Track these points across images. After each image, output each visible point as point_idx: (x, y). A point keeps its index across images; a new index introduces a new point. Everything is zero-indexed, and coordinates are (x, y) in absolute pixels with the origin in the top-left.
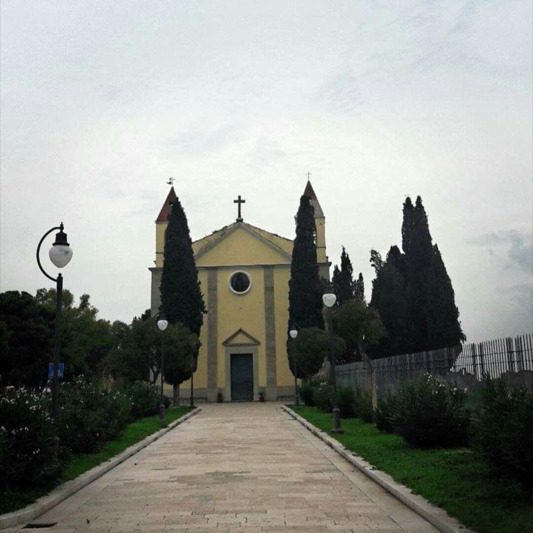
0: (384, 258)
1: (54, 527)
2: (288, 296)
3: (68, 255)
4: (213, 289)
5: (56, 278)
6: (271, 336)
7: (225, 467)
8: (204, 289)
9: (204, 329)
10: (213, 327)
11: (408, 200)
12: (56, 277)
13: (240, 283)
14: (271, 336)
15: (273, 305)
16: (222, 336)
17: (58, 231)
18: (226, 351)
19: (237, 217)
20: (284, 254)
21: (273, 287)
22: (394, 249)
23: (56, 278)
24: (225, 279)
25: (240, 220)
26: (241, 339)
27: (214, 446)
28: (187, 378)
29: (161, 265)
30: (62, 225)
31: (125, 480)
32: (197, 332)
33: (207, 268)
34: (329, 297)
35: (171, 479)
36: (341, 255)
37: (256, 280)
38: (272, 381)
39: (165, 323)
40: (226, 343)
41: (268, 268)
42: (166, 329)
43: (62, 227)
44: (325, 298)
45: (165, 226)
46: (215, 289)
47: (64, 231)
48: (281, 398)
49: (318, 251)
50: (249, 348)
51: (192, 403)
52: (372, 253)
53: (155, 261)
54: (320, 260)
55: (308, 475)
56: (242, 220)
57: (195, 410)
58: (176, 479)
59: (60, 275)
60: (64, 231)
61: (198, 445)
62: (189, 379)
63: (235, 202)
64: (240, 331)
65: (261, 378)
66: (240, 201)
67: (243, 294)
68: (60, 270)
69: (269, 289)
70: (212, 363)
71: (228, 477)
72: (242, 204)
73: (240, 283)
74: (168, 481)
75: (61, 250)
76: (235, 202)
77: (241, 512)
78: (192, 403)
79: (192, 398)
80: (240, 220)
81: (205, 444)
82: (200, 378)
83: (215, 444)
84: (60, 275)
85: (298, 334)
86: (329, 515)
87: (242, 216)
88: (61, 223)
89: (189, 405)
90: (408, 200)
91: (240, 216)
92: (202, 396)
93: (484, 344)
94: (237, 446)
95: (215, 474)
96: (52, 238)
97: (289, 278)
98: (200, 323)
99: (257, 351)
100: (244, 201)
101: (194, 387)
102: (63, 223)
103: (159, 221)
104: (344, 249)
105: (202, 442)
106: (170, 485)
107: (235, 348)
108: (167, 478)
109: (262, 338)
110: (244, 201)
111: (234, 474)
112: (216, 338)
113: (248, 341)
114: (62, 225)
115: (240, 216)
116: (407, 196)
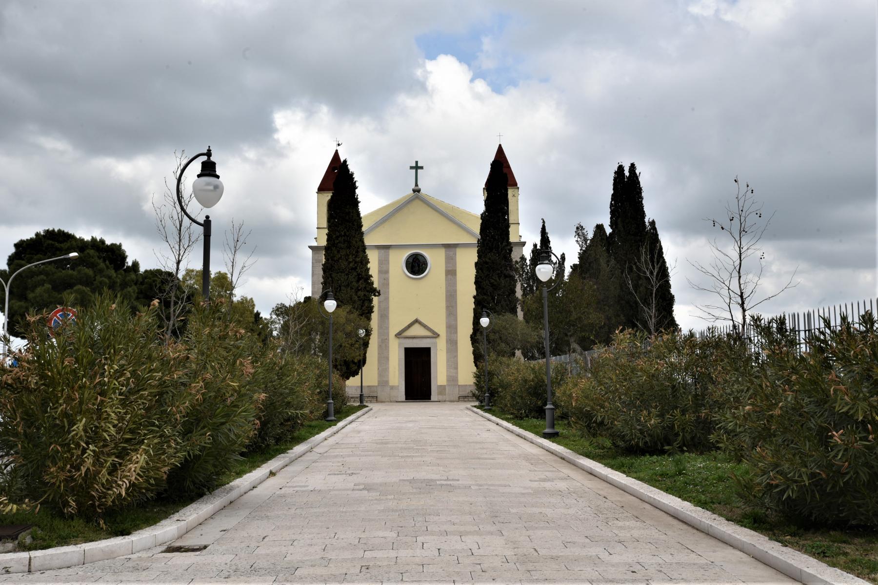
0: (590, 236)
1: (204, 551)
2: (473, 280)
3: (218, 190)
4: (384, 271)
5: (202, 222)
6: (452, 328)
7: (423, 474)
8: (373, 268)
9: (375, 316)
10: (384, 317)
11: (621, 168)
12: (201, 220)
13: (416, 265)
14: (452, 328)
15: (455, 291)
16: (395, 327)
17: (205, 158)
18: (400, 345)
19: (413, 186)
20: (469, 232)
21: (456, 270)
22: (600, 228)
23: (202, 222)
24: (398, 261)
25: (417, 191)
26: (416, 330)
27: (401, 448)
28: (355, 373)
29: (324, 243)
30: (209, 150)
31: (295, 487)
32: (369, 319)
33: (378, 247)
34: (543, 268)
35: (357, 487)
36: (541, 227)
37: (435, 260)
38: (453, 379)
39: (334, 304)
40: (398, 335)
41: (449, 247)
42: (333, 312)
43: (209, 154)
44: (539, 270)
45: (328, 196)
46: (387, 272)
47: (212, 159)
48: (463, 398)
49: (512, 229)
50: (428, 340)
51: (361, 401)
52: (577, 228)
53: (316, 238)
54: (513, 239)
55: (535, 485)
56: (419, 191)
57: (366, 409)
58: (362, 487)
59: (207, 217)
60: (212, 159)
61: (378, 446)
62: (357, 374)
63: (411, 168)
64: (416, 321)
65: (440, 374)
66: (417, 167)
67: (429, 270)
68: (207, 211)
69: (451, 273)
70: (384, 358)
71: (429, 486)
72: (419, 171)
73: (416, 265)
74: (353, 490)
75: (208, 184)
76: (411, 168)
77: (467, 533)
78: (361, 401)
79: (361, 396)
80: (417, 191)
81: (389, 446)
82: (370, 374)
83: (400, 446)
84: (207, 217)
85: (490, 322)
86: (592, 539)
87: (420, 186)
88: (208, 148)
89: (358, 404)
90: (621, 168)
91: (416, 185)
92: (372, 394)
93: (787, 317)
94: (430, 449)
95: (412, 481)
96: (196, 167)
97: (476, 259)
98: (370, 310)
99: (436, 344)
100: (422, 168)
101: (363, 385)
102: (211, 148)
103: (321, 189)
104: (544, 222)
105: (386, 443)
106: (357, 494)
107: (410, 340)
108: (351, 485)
109: (441, 330)
110: (422, 168)
111: (438, 482)
112: (388, 328)
113: (428, 334)
114: (209, 150)
115: (416, 185)
116: (620, 164)
